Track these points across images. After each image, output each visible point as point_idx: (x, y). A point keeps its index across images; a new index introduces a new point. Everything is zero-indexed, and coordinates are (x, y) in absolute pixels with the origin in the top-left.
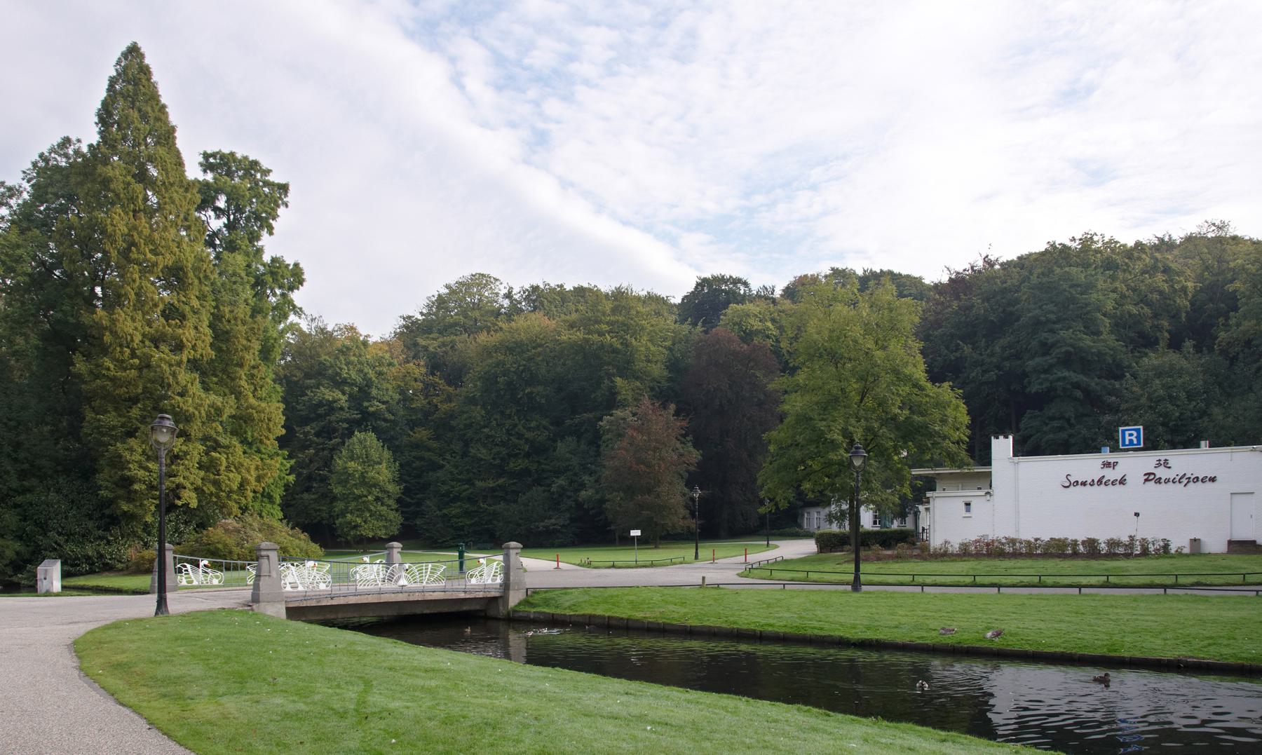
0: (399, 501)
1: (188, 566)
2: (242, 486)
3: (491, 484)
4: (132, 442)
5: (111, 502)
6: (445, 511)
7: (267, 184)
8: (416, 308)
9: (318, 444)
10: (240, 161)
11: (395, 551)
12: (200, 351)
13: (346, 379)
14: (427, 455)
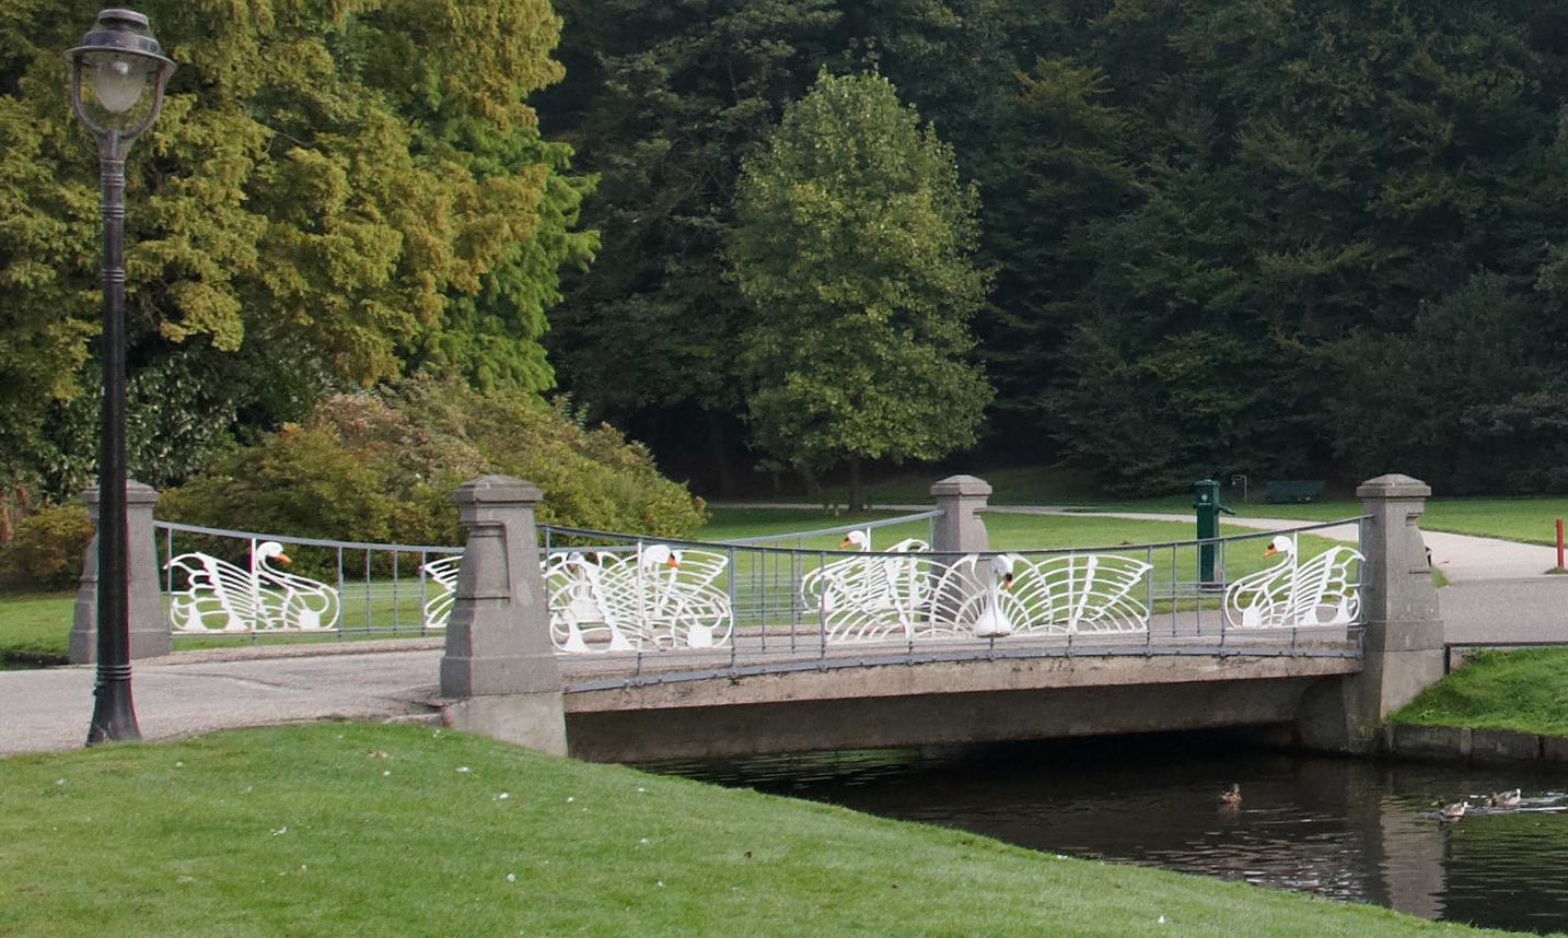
0: (979, 325)
1: (210, 563)
3: (1315, 263)
6: (1148, 363)
9: (681, 118)
11: (966, 508)
14: (1079, 156)
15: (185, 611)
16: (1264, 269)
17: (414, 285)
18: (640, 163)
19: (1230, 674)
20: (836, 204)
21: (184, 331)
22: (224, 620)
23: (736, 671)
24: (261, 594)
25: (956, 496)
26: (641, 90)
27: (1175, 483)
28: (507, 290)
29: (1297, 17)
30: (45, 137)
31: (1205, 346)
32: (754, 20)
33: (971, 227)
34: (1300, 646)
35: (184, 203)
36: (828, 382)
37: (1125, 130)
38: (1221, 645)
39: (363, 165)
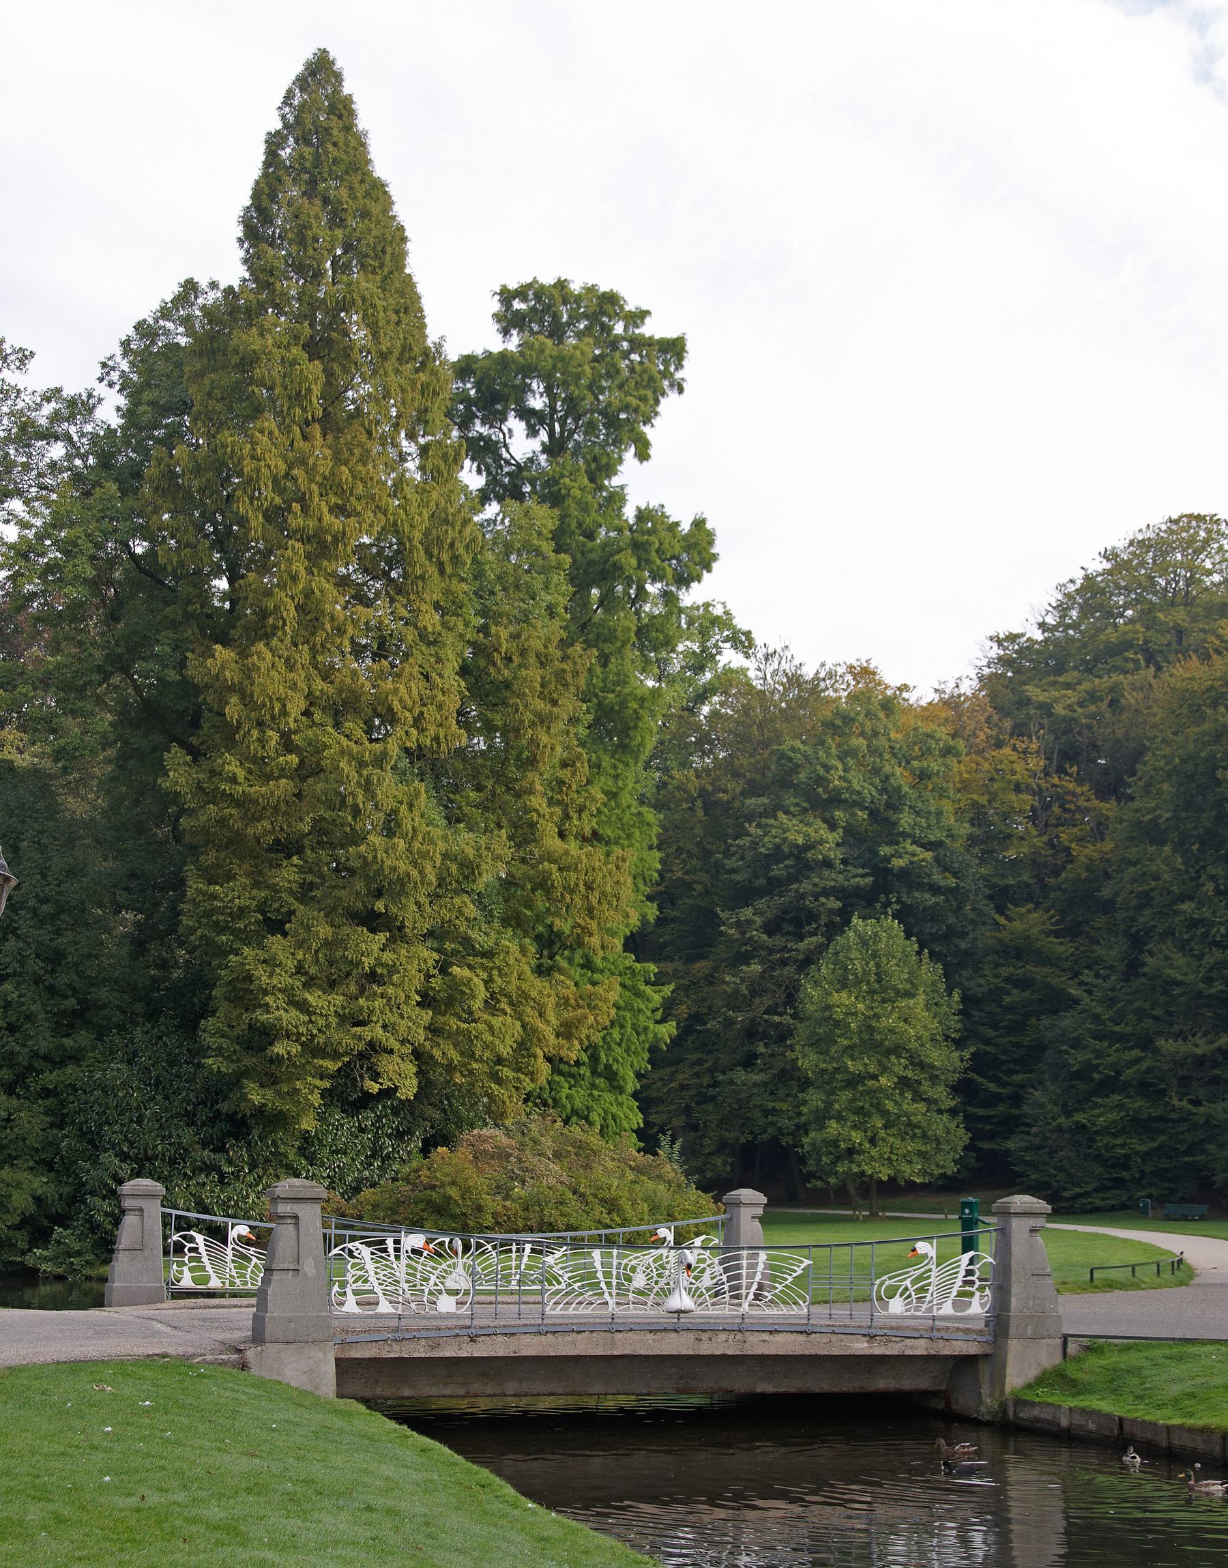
0: (962, 1088)
1: (200, 1238)
2: (522, 1047)
3: (1201, 1046)
4: (276, 943)
5: (227, 1086)
6: (1080, 1117)
7: (638, 343)
8: (1027, 609)
9: (771, 951)
10: (578, 299)
11: (746, 1214)
12: (432, 730)
13: (838, 791)
14: (1037, 972)
15: (181, 1272)
16: (1163, 1051)
17: (529, 1056)
18: (742, 980)
19: (878, 1350)
20: (861, 1006)
21: (378, 1086)
22: (208, 1279)
23: (474, 1332)
24: (233, 1261)
25: (738, 1204)
26: (744, 933)
27: (1101, 1203)
28: (611, 1061)
29: (1187, 871)
30: (299, 961)
31: (1120, 1106)
32: (815, 885)
33: (955, 1023)
34: (938, 1330)
35: (379, 1003)
36: (855, 1127)
37: (1072, 955)
38: (869, 1327)
39: (496, 978)
